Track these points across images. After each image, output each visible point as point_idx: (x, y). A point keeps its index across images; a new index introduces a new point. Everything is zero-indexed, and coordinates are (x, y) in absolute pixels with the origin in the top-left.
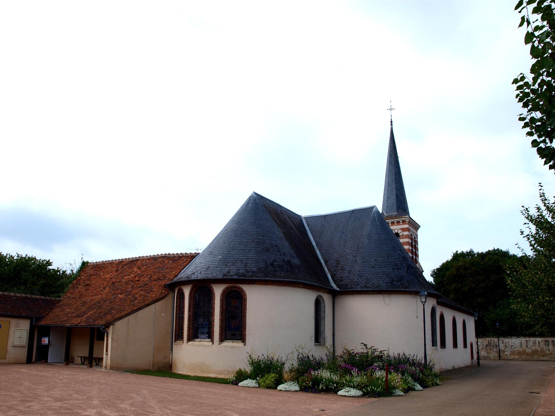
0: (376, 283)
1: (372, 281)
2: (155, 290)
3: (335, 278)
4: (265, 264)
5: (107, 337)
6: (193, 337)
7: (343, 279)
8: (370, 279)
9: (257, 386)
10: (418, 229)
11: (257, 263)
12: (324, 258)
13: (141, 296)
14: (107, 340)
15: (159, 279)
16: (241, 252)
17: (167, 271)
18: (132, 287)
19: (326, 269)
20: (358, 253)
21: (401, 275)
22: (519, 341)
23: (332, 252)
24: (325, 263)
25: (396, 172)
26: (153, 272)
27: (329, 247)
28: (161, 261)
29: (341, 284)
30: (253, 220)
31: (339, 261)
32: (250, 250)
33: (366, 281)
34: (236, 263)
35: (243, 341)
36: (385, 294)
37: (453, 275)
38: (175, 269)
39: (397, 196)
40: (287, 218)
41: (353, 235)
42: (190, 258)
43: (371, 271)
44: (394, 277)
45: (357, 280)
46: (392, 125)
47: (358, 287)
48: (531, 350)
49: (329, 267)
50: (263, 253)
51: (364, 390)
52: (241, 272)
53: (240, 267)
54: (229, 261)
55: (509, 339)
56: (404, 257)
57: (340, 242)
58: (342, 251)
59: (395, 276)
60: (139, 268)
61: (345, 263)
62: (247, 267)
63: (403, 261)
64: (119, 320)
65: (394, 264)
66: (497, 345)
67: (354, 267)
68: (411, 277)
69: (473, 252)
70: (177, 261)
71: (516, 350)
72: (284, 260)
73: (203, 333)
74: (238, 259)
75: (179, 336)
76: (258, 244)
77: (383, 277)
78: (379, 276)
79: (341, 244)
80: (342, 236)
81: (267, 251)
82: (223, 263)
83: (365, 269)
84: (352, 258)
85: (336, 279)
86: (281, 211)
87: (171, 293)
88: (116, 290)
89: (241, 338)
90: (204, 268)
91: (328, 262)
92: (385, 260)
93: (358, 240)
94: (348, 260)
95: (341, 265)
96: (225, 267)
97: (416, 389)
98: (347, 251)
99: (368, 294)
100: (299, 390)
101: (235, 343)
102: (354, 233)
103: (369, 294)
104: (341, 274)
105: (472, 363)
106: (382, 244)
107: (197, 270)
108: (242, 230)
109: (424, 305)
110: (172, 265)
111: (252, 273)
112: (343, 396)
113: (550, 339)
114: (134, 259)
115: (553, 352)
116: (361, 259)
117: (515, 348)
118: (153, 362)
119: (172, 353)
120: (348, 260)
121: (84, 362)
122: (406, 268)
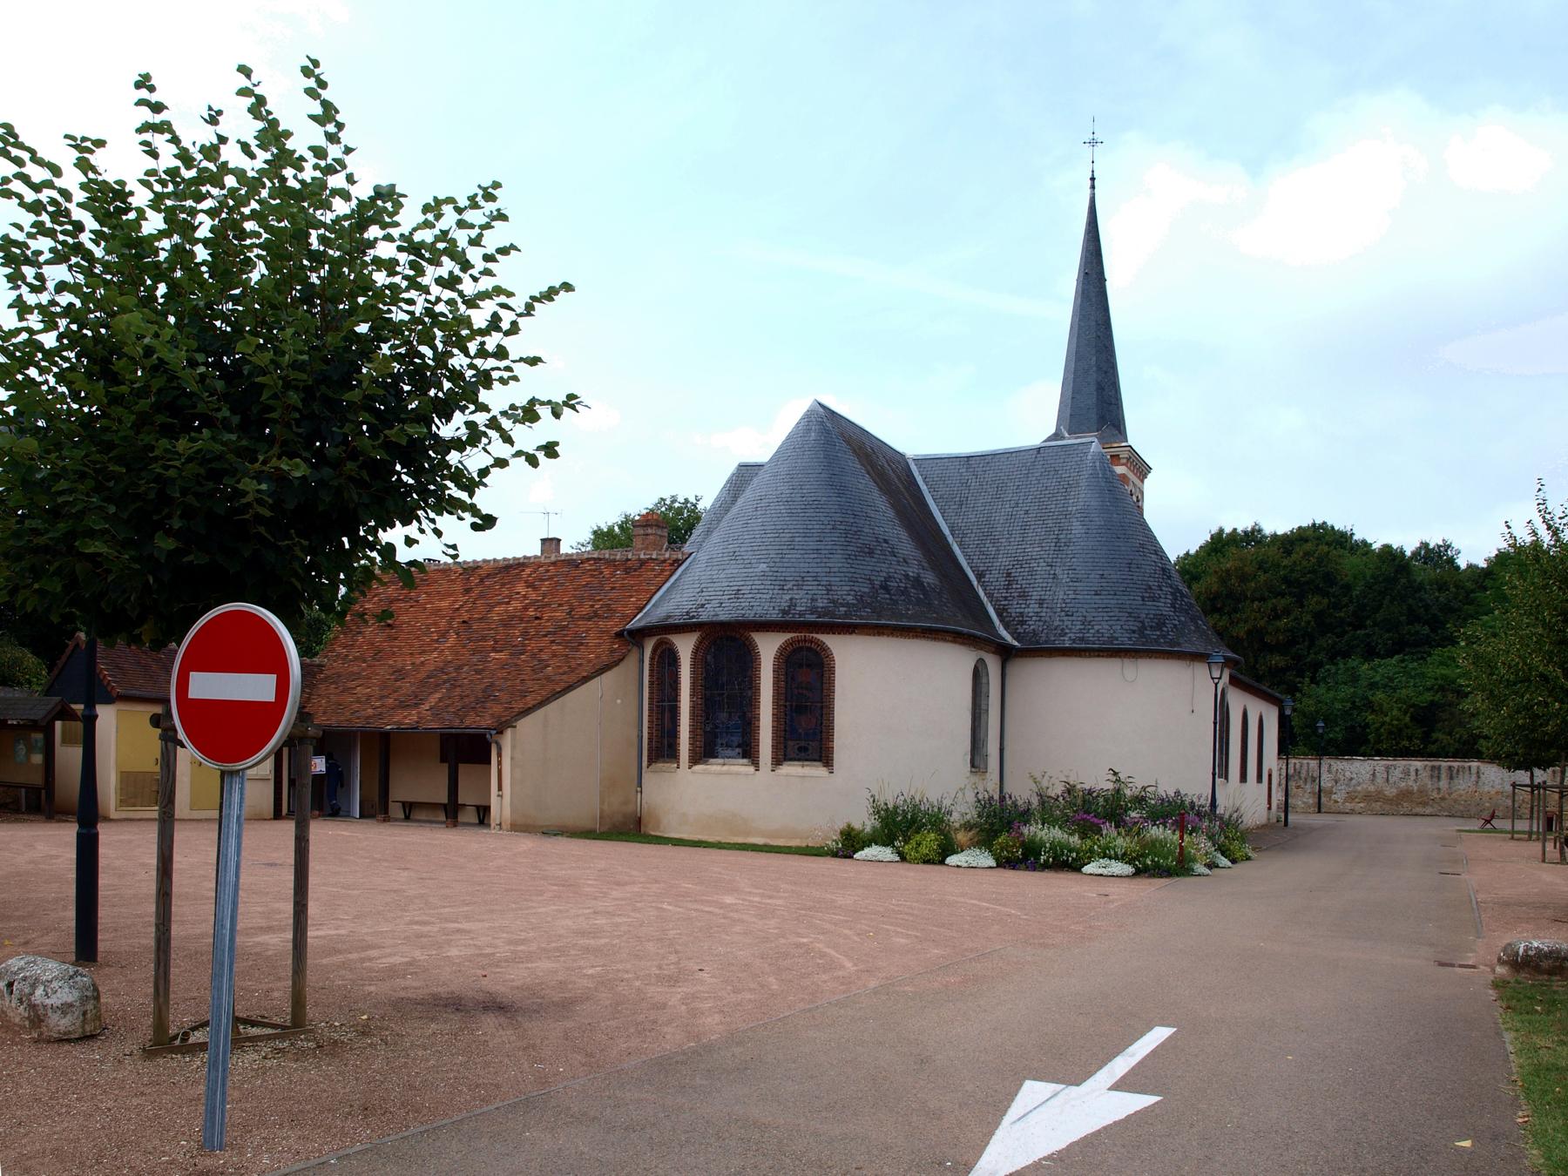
0: (1106, 631)
1: (1096, 627)
2: (592, 642)
3: (1007, 617)
4: (870, 586)
5: (499, 755)
6: (705, 752)
7: (1025, 619)
8: (1090, 621)
9: (898, 859)
10: (1145, 476)
11: (852, 584)
12: (973, 565)
13: (555, 656)
14: (500, 763)
15: (596, 614)
16: (812, 556)
17: (612, 595)
18: (525, 634)
19: (981, 593)
20: (1060, 556)
21: (1160, 613)
22: (1368, 768)
23: (993, 553)
24: (977, 578)
25: (1100, 322)
26: (574, 596)
27: (985, 538)
28: (590, 570)
29: (1022, 631)
30: (826, 476)
31: (1013, 575)
32: (831, 551)
33: (1082, 627)
34: (806, 583)
35: (827, 763)
36: (1125, 657)
37: (1211, 593)
38: (636, 591)
39: (1100, 388)
40: (886, 465)
41: (1044, 511)
42: (672, 565)
43: (1093, 602)
44: (1146, 618)
45: (1061, 623)
46: (1093, 187)
47: (1064, 640)
48: (1395, 791)
49: (988, 588)
50: (862, 558)
51: (1137, 863)
52: (821, 605)
53: (816, 592)
54: (787, 579)
55: (1345, 763)
56: (1163, 570)
57: (1011, 529)
58: (1018, 551)
59: (1147, 614)
60: (530, 585)
61: (1028, 581)
62: (832, 592)
63: (1163, 579)
64: (524, 716)
65: (1144, 587)
66: (1315, 775)
67: (1050, 590)
68: (1183, 619)
69: (1260, 531)
70: (635, 570)
71: (1359, 788)
72: (908, 575)
73: (728, 746)
74: (808, 572)
75: (663, 748)
76: (847, 537)
77: (1121, 618)
78: (1112, 614)
79: (1014, 532)
80: (1014, 513)
81: (869, 553)
82: (773, 583)
83: (1078, 597)
84: (1044, 568)
85: (1008, 619)
86: (871, 448)
87: (635, 649)
88: (480, 641)
89: (821, 756)
90: (726, 593)
91: (984, 577)
92: (1124, 577)
93: (1057, 525)
94: (1034, 573)
95: (1019, 586)
96: (781, 592)
97: (1220, 865)
98: (1030, 550)
99: (1086, 657)
100: (995, 865)
101: (808, 768)
102: (1044, 507)
103: (1090, 656)
104: (1020, 608)
105: (1269, 819)
106: (1114, 536)
107: (708, 598)
108: (804, 499)
109: (1216, 684)
110: (626, 582)
111: (845, 609)
112: (1096, 875)
113: (1444, 764)
114: (511, 562)
115: (1447, 796)
116: (1066, 572)
117: (1359, 784)
118: (600, 813)
119: (641, 792)
120: (1034, 573)
121: (409, 814)
122: (1171, 597)
